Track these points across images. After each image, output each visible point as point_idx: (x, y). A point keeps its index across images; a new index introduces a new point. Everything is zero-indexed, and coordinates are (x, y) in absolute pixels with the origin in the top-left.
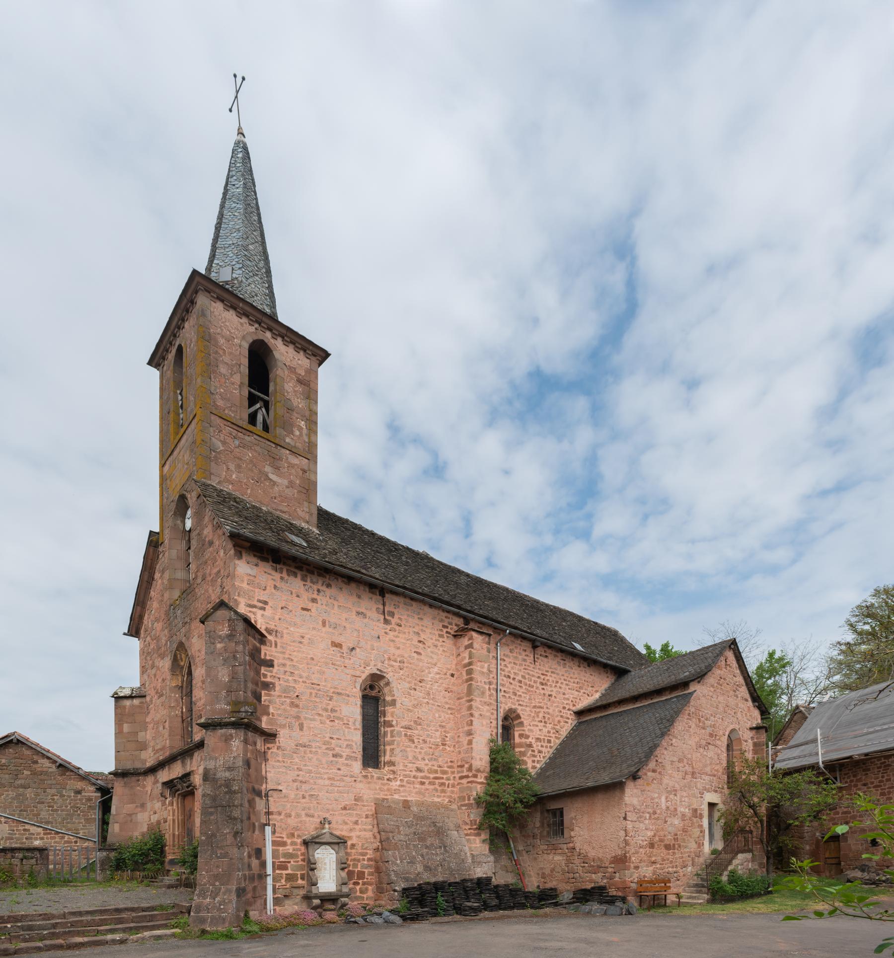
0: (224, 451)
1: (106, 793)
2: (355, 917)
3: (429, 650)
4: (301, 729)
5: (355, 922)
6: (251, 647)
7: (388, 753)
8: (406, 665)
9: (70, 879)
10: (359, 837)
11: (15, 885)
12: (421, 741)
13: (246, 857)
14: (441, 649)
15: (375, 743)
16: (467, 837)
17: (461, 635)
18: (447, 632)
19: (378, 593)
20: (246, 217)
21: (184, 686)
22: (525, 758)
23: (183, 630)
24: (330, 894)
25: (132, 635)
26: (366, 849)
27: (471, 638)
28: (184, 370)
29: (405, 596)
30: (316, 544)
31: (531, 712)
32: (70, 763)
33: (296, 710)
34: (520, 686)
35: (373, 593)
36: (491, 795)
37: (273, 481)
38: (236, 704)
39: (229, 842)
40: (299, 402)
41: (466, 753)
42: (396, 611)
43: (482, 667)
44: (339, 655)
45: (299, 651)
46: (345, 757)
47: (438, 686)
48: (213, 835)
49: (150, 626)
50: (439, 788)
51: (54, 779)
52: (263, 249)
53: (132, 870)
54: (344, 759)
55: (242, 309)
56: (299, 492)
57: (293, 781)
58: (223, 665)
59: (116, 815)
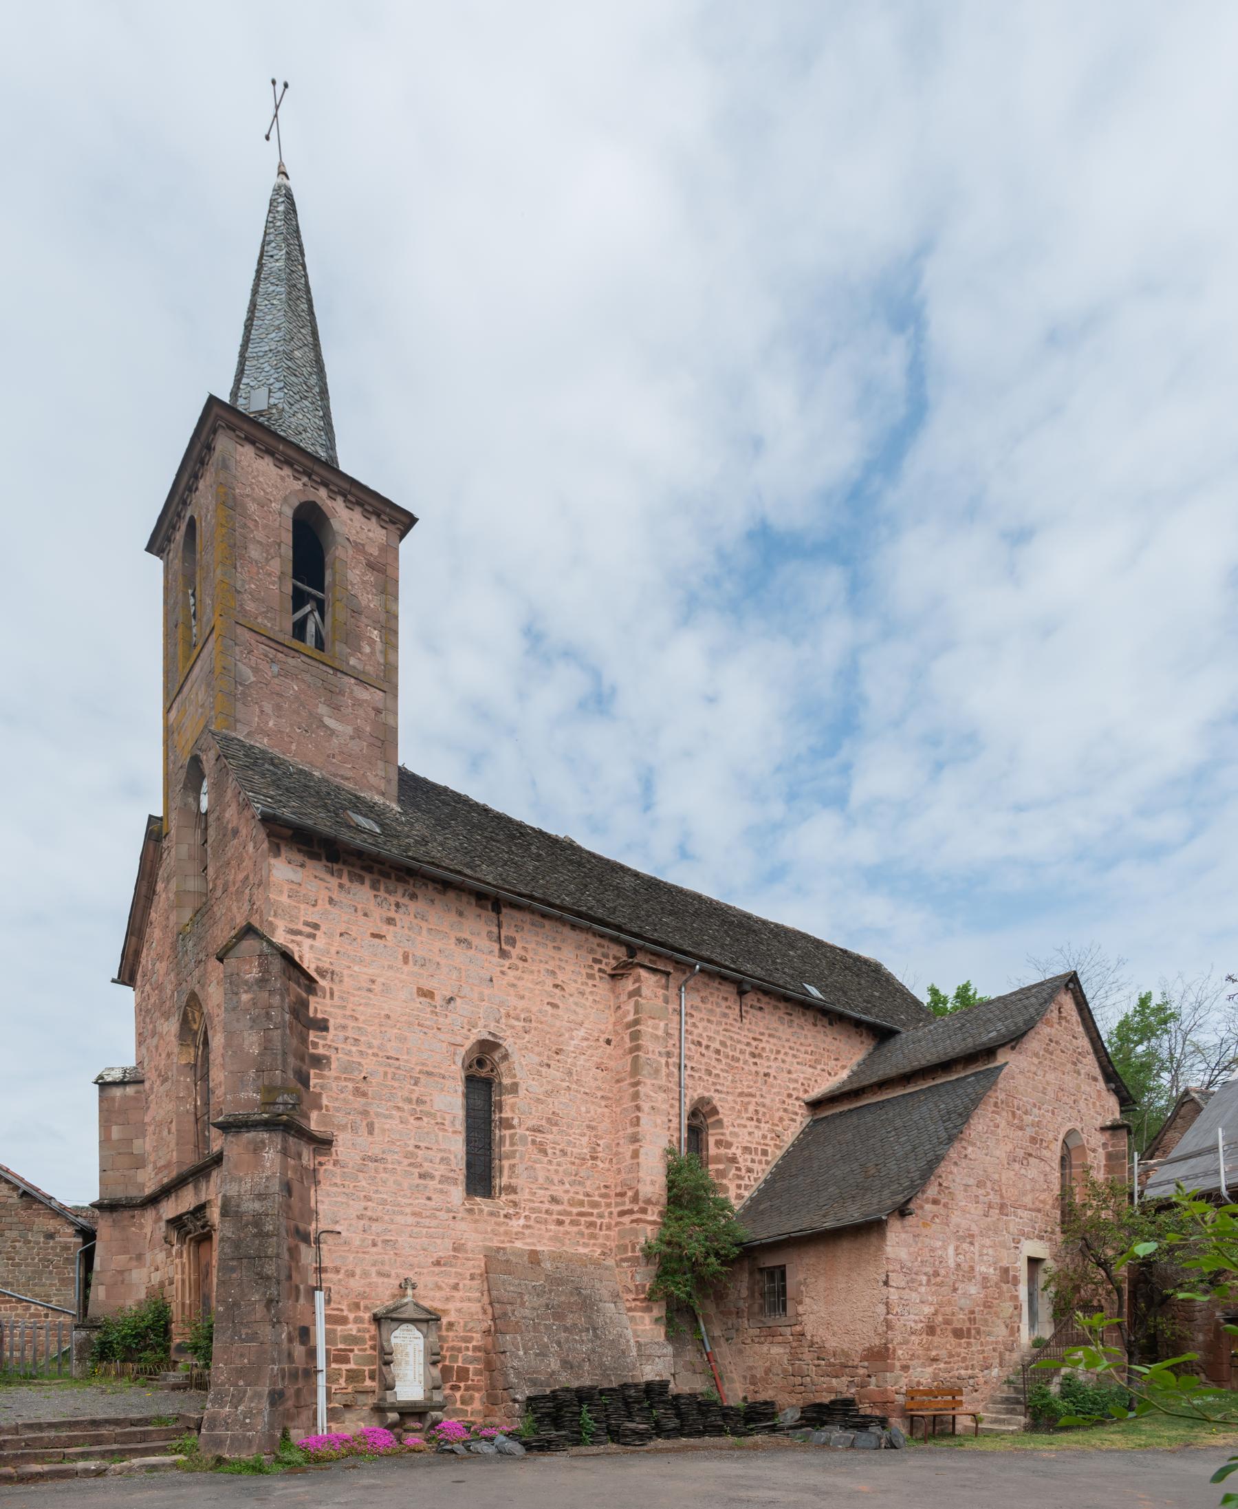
4: (371, 1132)
7: (506, 1172)
10: (459, 1311)
21: (199, 1064)
25: (124, 983)
33: (362, 1100)
42: (518, 936)
44: (429, 1010)
45: (366, 1005)
46: (438, 1178)
50: (586, 1231)
54: (436, 1182)
55: (283, 453)
57: (360, 1217)
58: (251, 1028)
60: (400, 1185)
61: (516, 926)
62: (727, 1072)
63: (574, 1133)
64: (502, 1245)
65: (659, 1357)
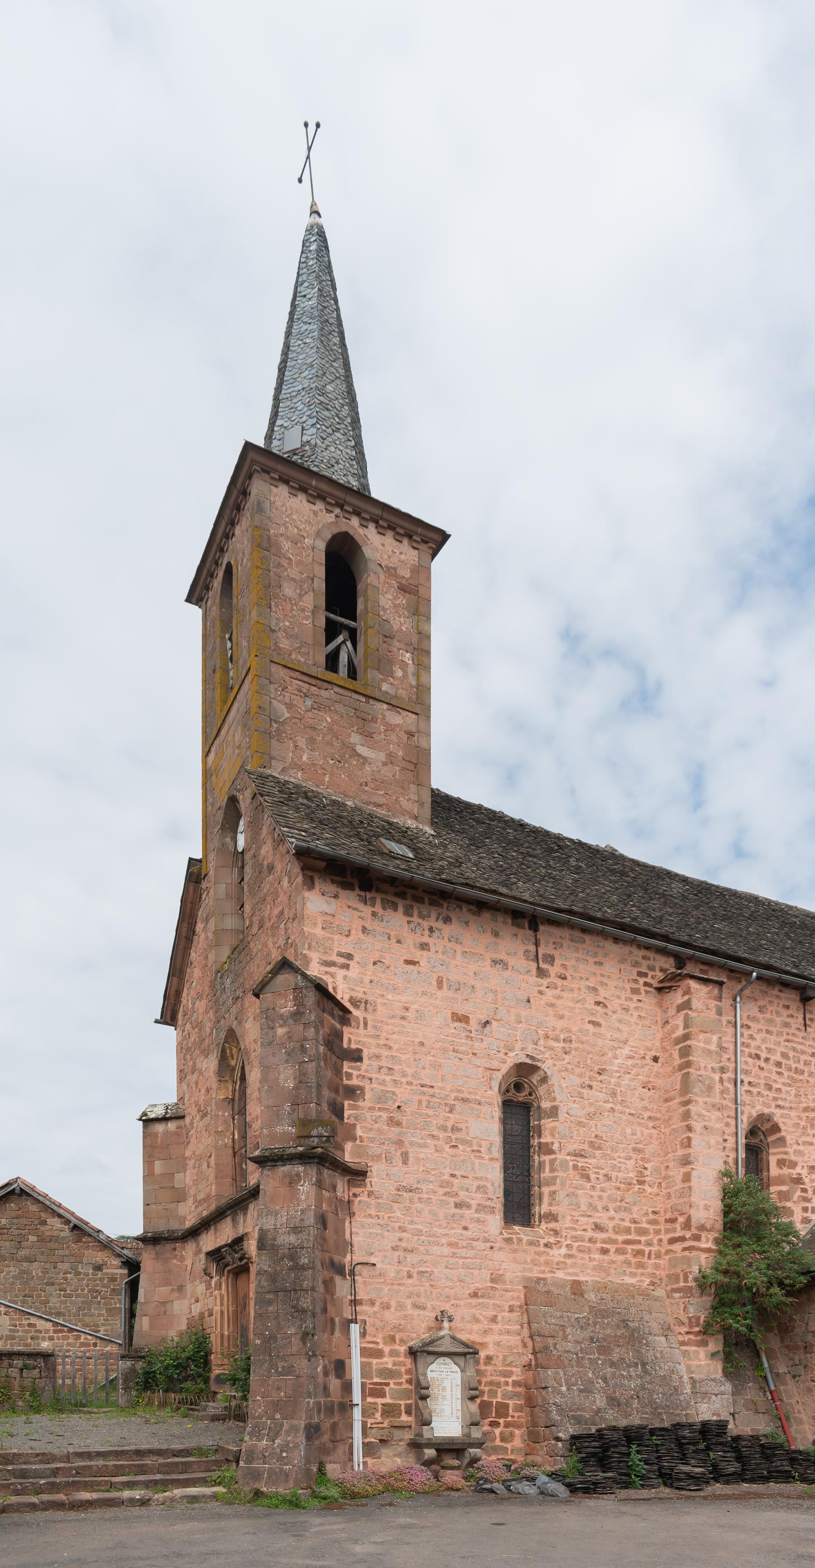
0: (290, 719)
1: (133, 1266)
2: (492, 1482)
3: (614, 1016)
4: (405, 1162)
5: (492, 1491)
6: (327, 1030)
7: (546, 1199)
8: (574, 1045)
9: (84, 1401)
10: (498, 1344)
11: (13, 1408)
12: (601, 1177)
13: (321, 1374)
14: (636, 1014)
15: (524, 1182)
16: (684, 1348)
17: (670, 988)
18: (646, 984)
19: (527, 925)
20: (322, 342)
21: (237, 1098)
22: (788, 1204)
23: (234, 1010)
24: (451, 1440)
25: (166, 1023)
26: (509, 1365)
27: (688, 992)
28: (234, 601)
29: (572, 926)
30: (428, 853)
31: (800, 1118)
32: (87, 1224)
33: (397, 1130)
34: (779, 1073)
35: (519, 926)
36: (726, 1272)
37: (364, 758)
38: (305, 1124)
39: (294, 1349)
40: (401, 623)
41: (680, 1196)
42: (556, 954)
43: (708, 1041)
45: (400, 1033)
46: (474, 1207)
47: (630, 1080)
48: (272, 1338)
49: (190, 1006)
50: (633, 1260)
51: (68, 1248)
52: (347, 387)
53: (166, 1391)
54: (473, 1211)
55: (316, 488)
56: (403, 769)
57: (394, 1249)
58: (287, 1061)
59: (145, 1303)
60: (435, 1214)
61: (554, 943)
62: (790, 1085)
63: (619, 1157)
64: (542, 1276)
65: (716, 1395)
